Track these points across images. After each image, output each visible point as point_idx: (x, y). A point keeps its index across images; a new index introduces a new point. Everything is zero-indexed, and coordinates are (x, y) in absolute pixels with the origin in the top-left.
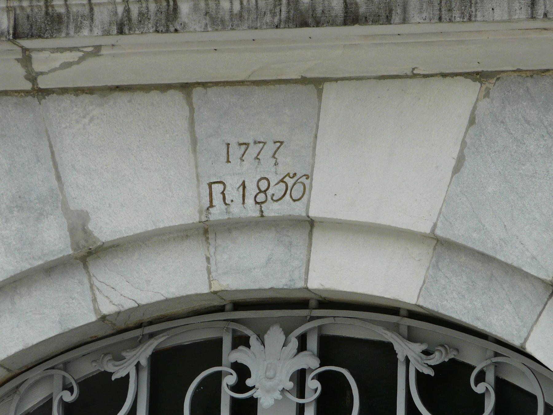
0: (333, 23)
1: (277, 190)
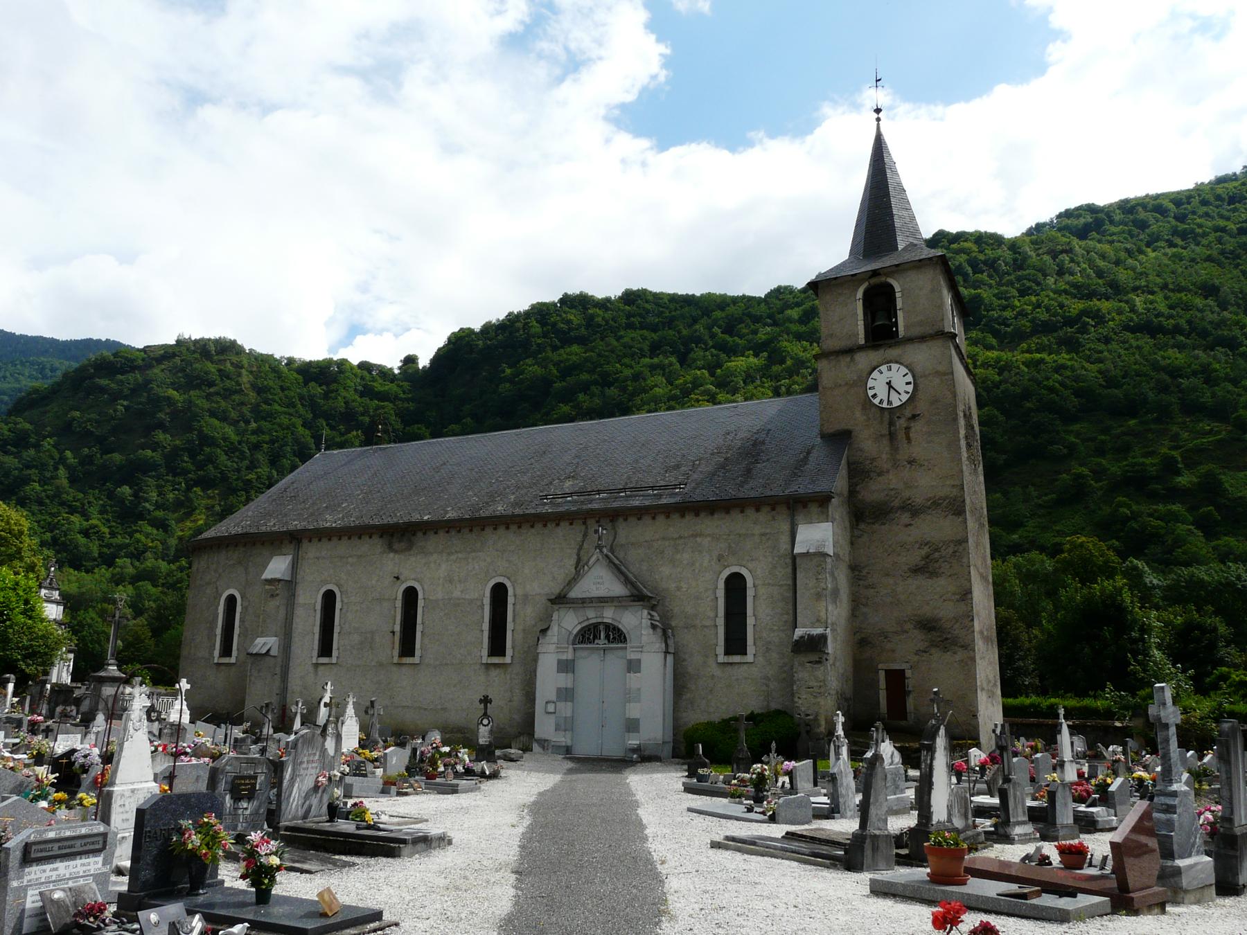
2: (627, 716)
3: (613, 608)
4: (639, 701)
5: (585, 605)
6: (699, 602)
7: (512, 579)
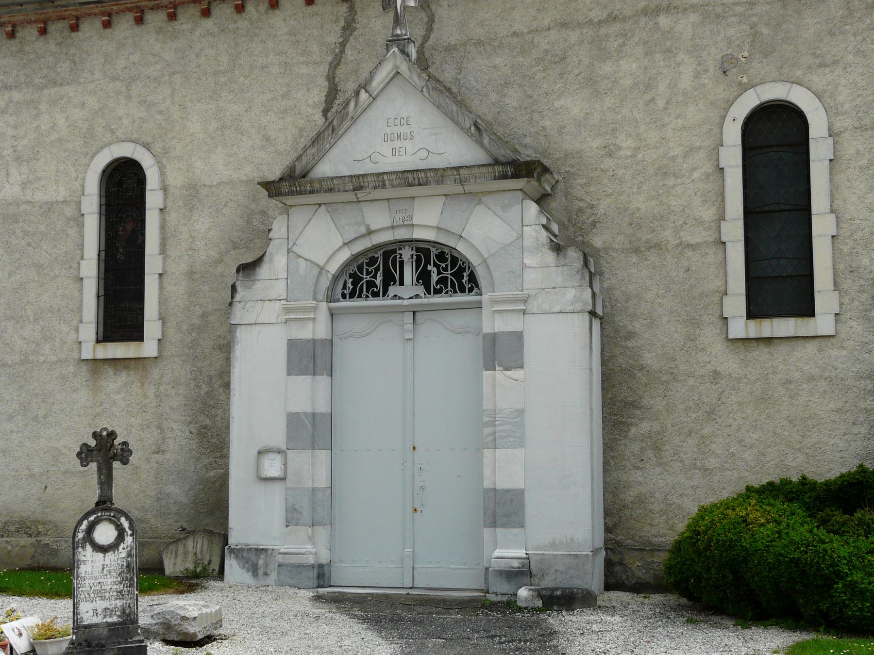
0: (416, 186)
1: (406, 219)
2: (487, 484)
3: (442, 199)
4: (519, 442)
5: (361, 195)
6: (671, 182)
7: (158, 147)
